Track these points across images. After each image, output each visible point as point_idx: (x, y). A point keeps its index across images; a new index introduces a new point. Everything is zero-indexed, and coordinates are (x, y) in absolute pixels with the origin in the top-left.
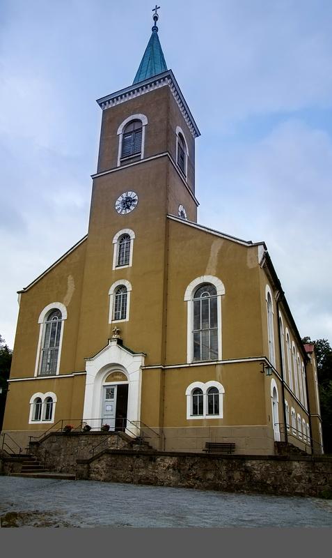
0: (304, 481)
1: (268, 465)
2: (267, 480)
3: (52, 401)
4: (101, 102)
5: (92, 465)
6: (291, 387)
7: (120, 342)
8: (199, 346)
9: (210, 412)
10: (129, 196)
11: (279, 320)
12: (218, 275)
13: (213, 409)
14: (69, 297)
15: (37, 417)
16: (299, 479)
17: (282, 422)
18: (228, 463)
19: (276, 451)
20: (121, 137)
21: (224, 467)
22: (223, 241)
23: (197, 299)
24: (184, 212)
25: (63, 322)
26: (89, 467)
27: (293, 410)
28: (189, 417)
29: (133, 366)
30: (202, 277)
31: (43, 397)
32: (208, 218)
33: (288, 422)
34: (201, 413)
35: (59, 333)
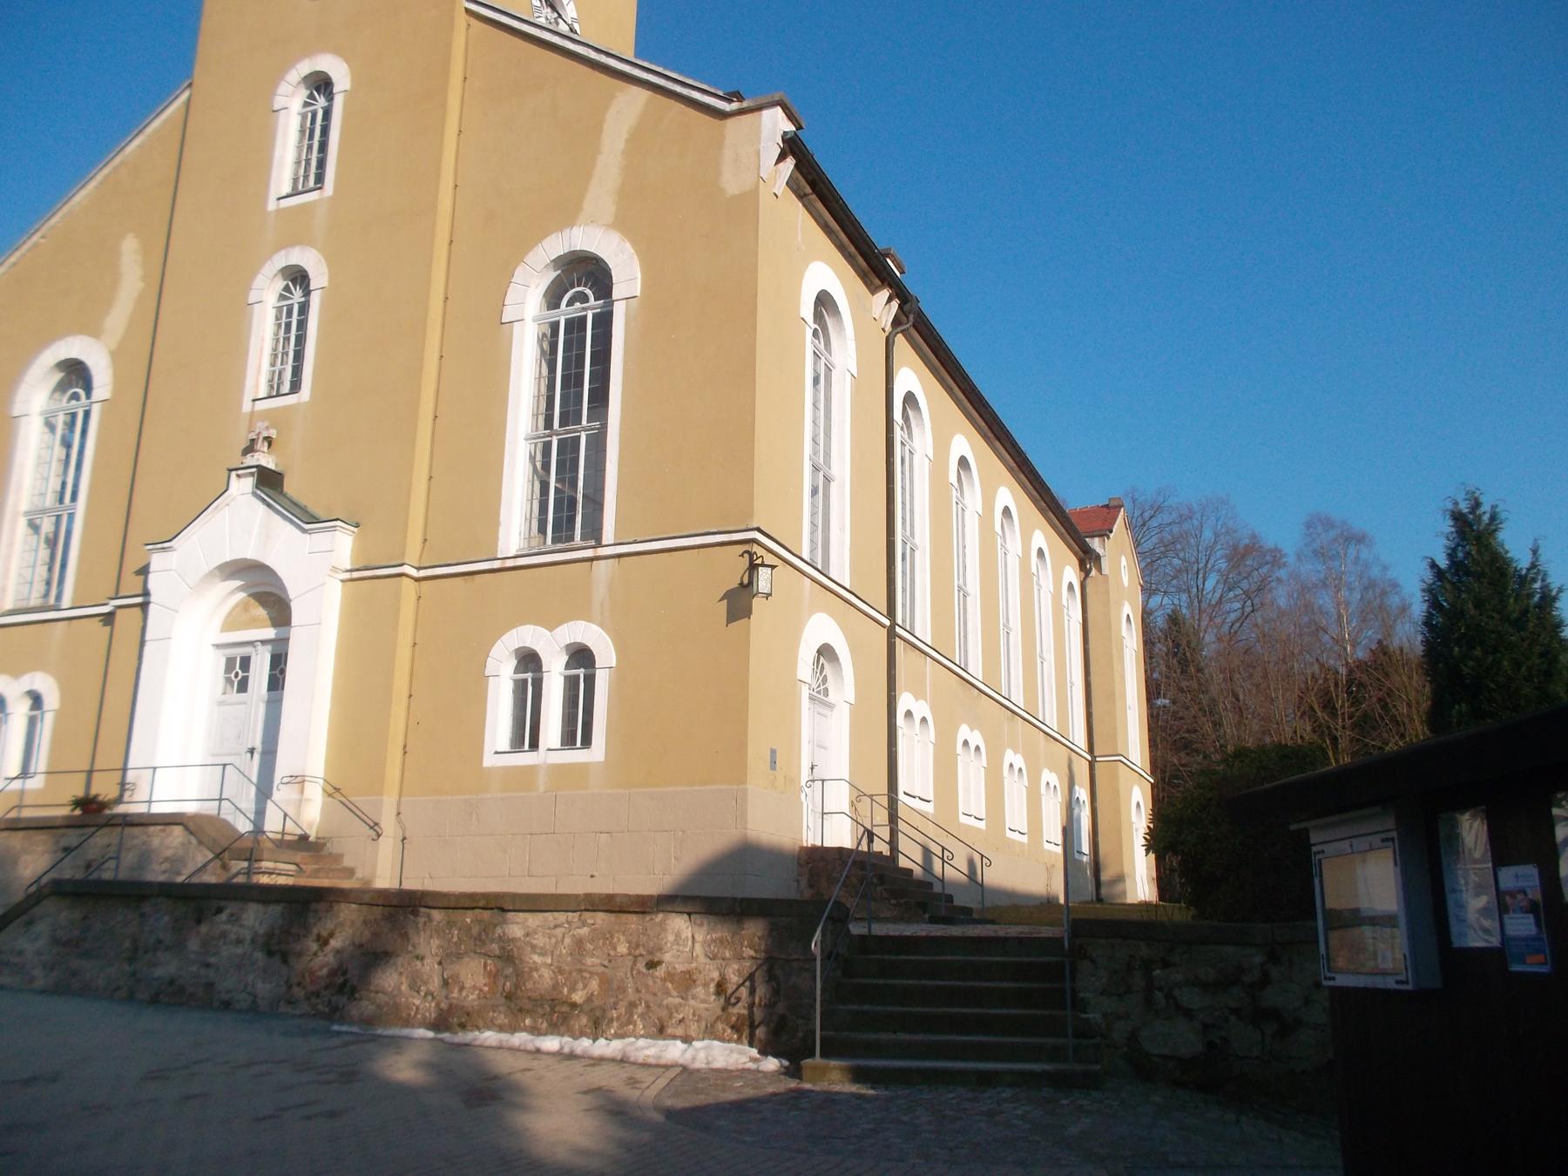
0: (700, 991)
1: (585, 931)
2: (573, 989)
7: (269, 481)
12: (622, 224)
14: (118, 318)
15: (526, 733)
16: (686, 981)
18: (451, 924)
19: (804, 883)
21: (435, 942)
22: (643, 94)
23: (553, 315)
25: (96, 411)
28: (489, 760)
30: (567, 232)
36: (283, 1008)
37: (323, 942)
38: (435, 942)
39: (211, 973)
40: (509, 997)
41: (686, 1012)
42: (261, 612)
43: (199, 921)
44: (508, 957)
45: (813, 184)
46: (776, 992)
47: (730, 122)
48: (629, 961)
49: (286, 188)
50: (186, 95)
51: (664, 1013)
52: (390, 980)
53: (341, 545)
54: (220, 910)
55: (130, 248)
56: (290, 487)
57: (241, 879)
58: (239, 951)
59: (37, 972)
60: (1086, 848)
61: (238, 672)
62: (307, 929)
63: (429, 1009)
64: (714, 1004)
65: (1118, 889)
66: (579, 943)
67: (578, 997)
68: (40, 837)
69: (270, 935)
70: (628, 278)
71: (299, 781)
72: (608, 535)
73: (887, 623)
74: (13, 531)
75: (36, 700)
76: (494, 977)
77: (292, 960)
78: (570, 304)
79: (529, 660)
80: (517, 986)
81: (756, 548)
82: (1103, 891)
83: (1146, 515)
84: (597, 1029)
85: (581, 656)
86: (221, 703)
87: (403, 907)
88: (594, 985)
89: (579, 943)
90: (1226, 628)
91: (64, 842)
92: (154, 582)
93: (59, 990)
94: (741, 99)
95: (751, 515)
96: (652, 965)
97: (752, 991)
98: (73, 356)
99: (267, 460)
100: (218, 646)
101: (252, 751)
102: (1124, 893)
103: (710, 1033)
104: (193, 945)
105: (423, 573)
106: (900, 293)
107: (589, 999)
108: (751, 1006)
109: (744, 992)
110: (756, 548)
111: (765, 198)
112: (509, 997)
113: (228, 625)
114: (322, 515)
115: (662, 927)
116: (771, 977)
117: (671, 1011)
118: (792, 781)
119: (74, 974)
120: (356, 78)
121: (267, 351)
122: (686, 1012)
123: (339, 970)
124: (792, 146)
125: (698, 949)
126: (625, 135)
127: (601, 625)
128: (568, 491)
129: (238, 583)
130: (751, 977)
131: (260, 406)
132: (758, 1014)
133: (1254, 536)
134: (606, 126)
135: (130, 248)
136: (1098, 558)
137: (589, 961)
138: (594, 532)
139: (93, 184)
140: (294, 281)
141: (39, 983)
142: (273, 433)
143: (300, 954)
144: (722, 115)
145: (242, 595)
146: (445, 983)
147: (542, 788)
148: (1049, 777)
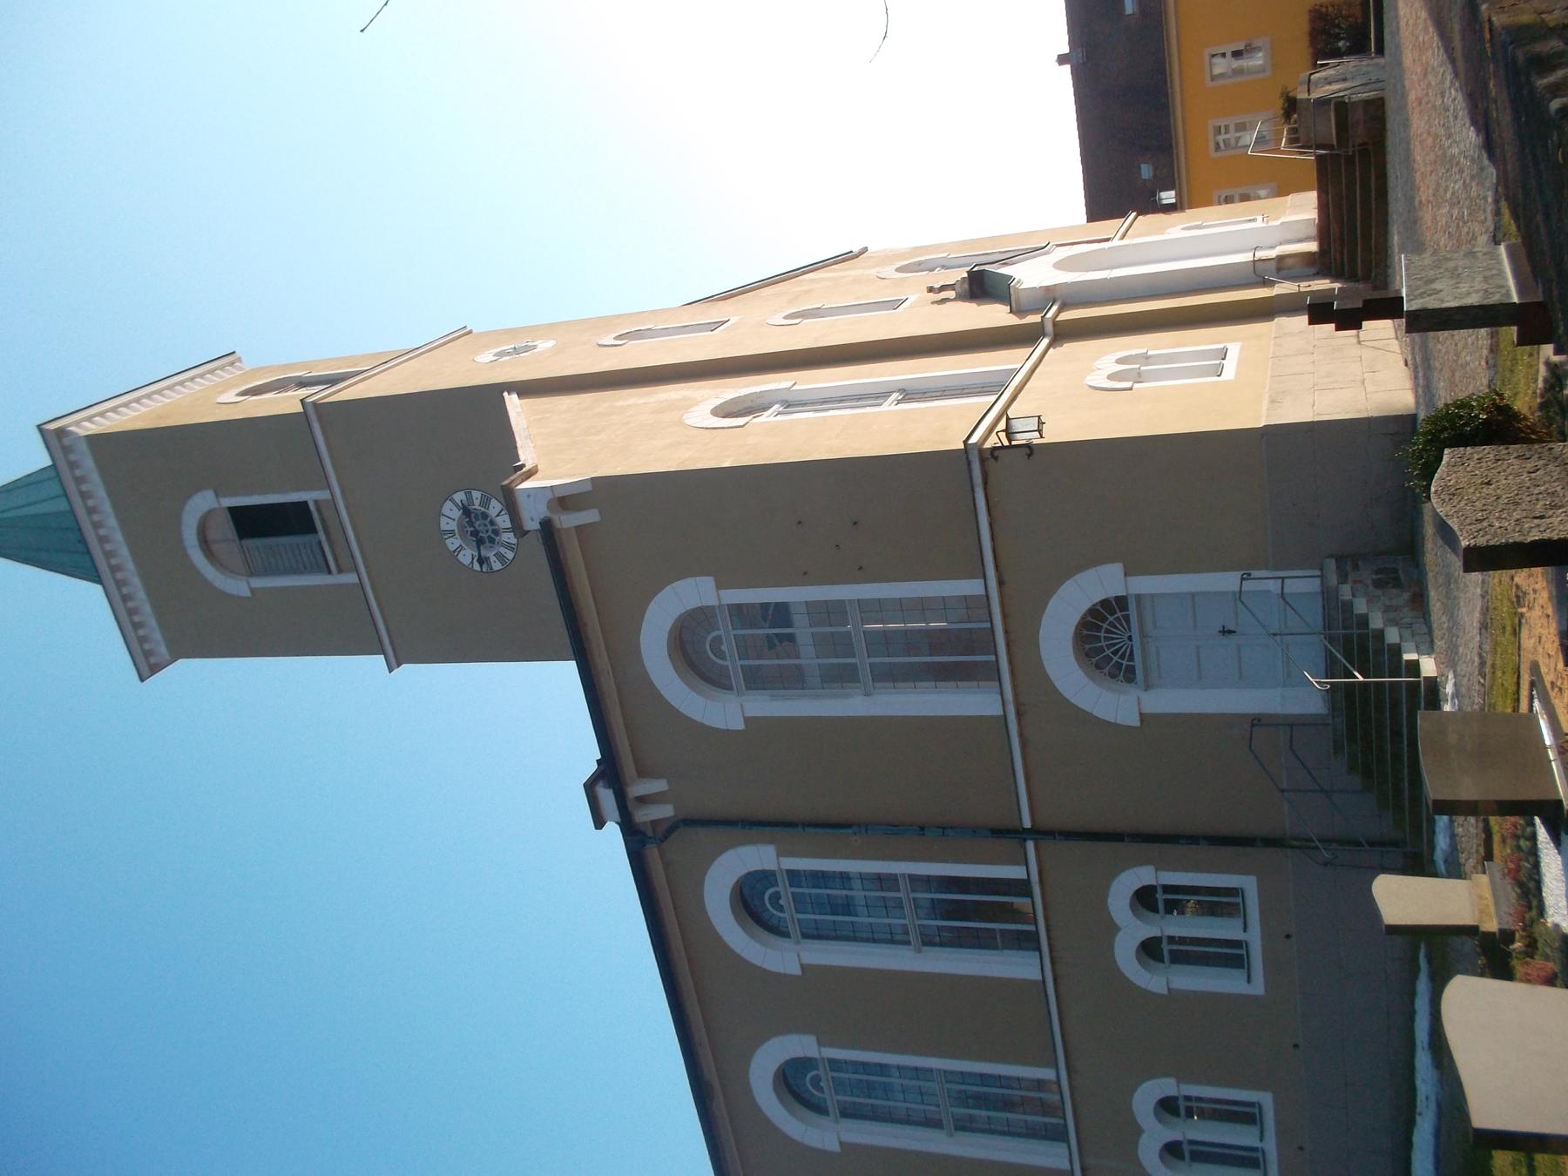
3: (1175, 1099)
4: (147, 666)
20: (258, 583)
31: (1132, 930)
32: (1446, 451)
35: (865, 1067)
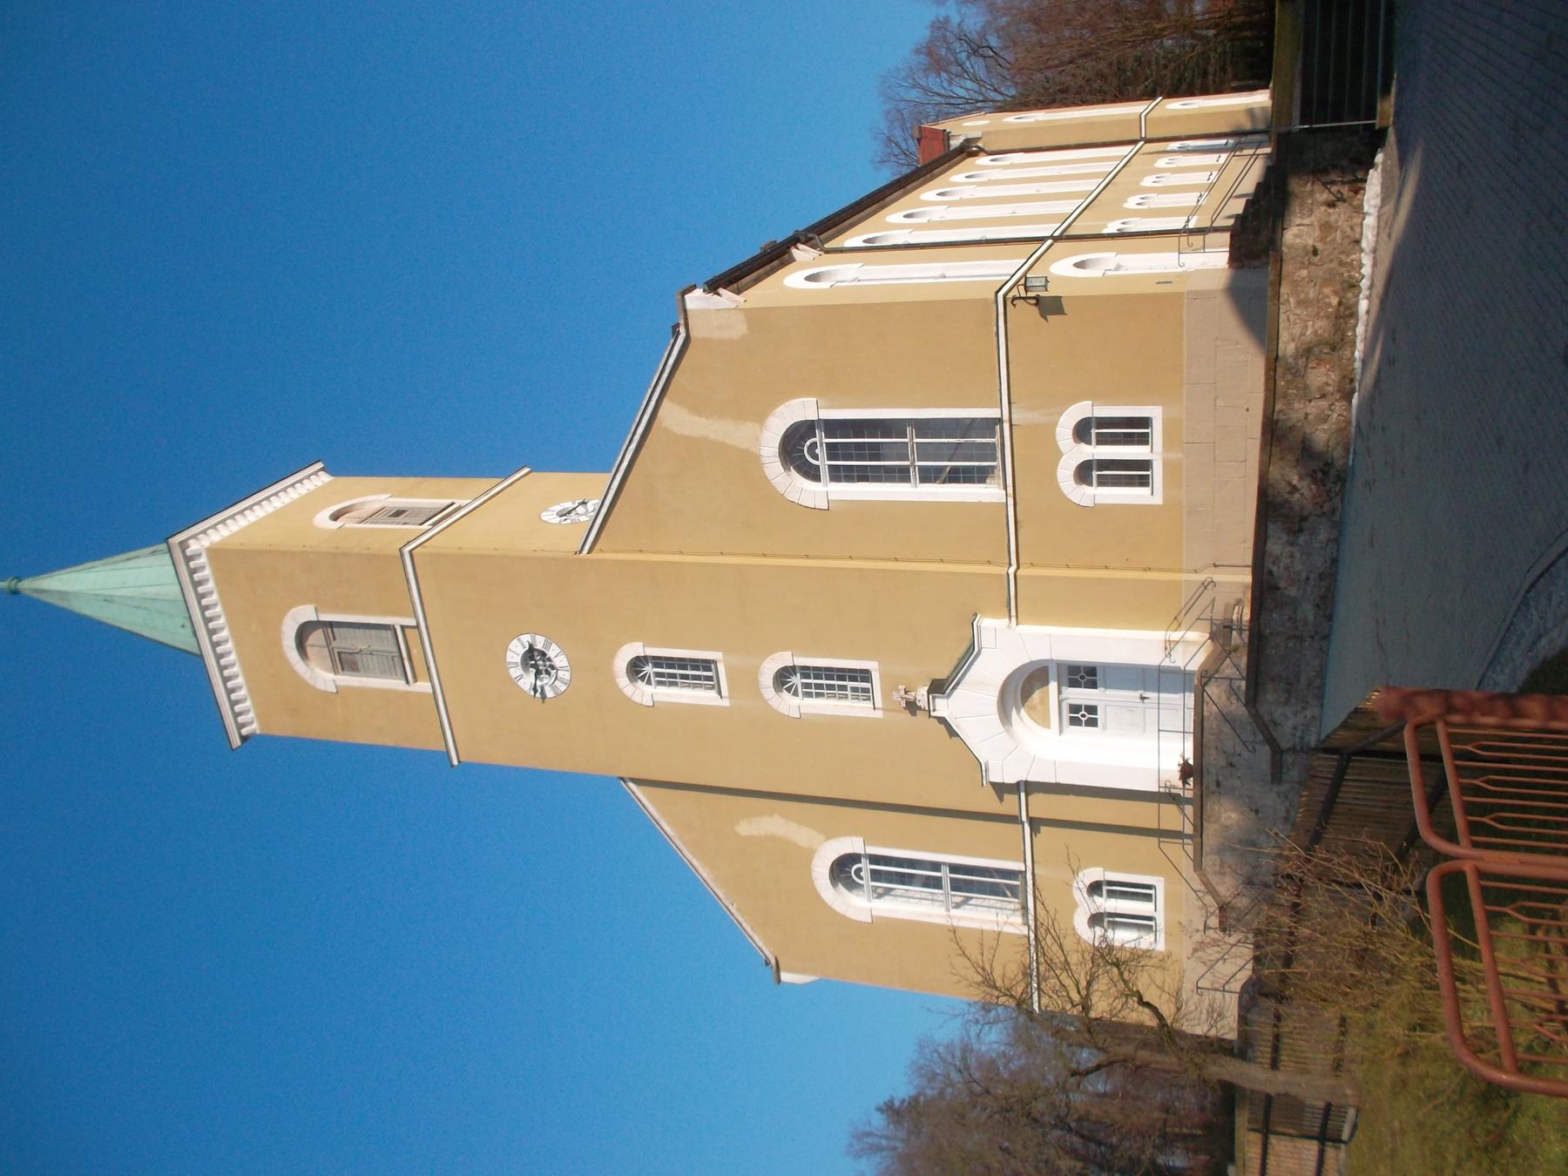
0: (1332, 219)
2: (1329, 305)
5: (1284, 745)
6: (1068, 207)
7: (939, 688)
8: (955, 470)
9: (1143, 440)
10: (518, 659)
11: (871, 248)
12: (761, 417)
13: (1135, 431)
16: (1326, 227)
17: (1173, 240)
18: (1285, 396)
22: (666, 403)
23: (824, 473)
24: (558, 508)
26: (1293, 750)
27: (1132, 203)
28: (1158, 500)
29: (1008, 643)
33: (1178, 223)
34: (1145, 465)
36: (1336, 518)
37: (1294, 489)
38: (1296, 405)
39: (1313, 576)
40: (1333, 349)
41: (1346, 226)
42: (1037, 695)
43: (1277, 588)
44: (1307, 352)
45: (733, 279)
46: (1334, 167)
47: (693, 334)
48: (1312, 268)
49: (713, 693)
50: (631, 785)
51: (1346, 241)
52: (1321, 436)
53: (991, 627)
54: (1271, 572)
55: (745, 828)
56: (942, 674)
57: (1246, 635)
58: (1298, 555)
59: (1309, 713)
60: (1223, 141)
61: (1084, 716)
62: (1286, 502)
63: (1339, 406)
64: (1342, 208)
65: (1258, 113)
66: (1299, 303)
67: (1335, 301)
68: (1208, 806)
69: (1289, 531)
70: (804, 409)
71: (1169, 646)
72: (993, 413)
73: (1049, 242)
74: (960, 919)
75: (1095, 888)
76: (1320, 361)
77: (1306, 513)
78: (816, 457)
79: (1084, 472)
80: (1326, 344)
81: (1010, 296)
82: (1261, 126)
83: (897, 151)
84: (1354, 286)
85: (1082, 432)
86: (1105, 728)
87: (1274, 433)
88: (1327, 291)
89: (1299, 303)
90: (1005, 73)
91: (1213, 787)
92: (1011, 779)
93: (1320, 694)
94: (678, 325)
95: (985, 301)
96: (1315, 252)
97: (1334, 183)
98: (827, 872)
99: (921, 695)
100: (1061, 731)
101: (1143, 698)
102: (1263, 109)
103: (1359, 210)
104: (1293, 592)
105: (1014, 561)
106: (794, 240)
107: (1336, 293)
108: (1343, 183)
109: (1334, 189)
110: (1010, 296)
111: (747, 305)
112: (1333, 349)
113: (1045, 723)
114: (967, 644)
115: (1291, 247)
116: (1325, 171)
117: (1345, 237)
118: (1179, 275)
119: (1310, 684)
120: (633, 638)
121: (833, 702)
122: (1346, 226)
123: (1312, 476)
124: (713, 286)
125: (1306, 221)
126: (696, 418)
127: (1060, 414)
128: (944, 475)
129: (1014, 712)
130: (1325, 184)
131: (879, 703)
132: (1349, 177)
133: (918, 51)
134: (687, 433)
135: (745, 828)
136: (967, 141)
137: (1312, 295)
138: (990, 425)
139: (695, 862)
140: (784, 684)
141: (1316, 712)
142: (902, 687)
143: (1302, 508)
144: (687, 339)
145: (1023, 711)
146: (1323, 396)
147: (1181, 455)
148: (1162, 162)
